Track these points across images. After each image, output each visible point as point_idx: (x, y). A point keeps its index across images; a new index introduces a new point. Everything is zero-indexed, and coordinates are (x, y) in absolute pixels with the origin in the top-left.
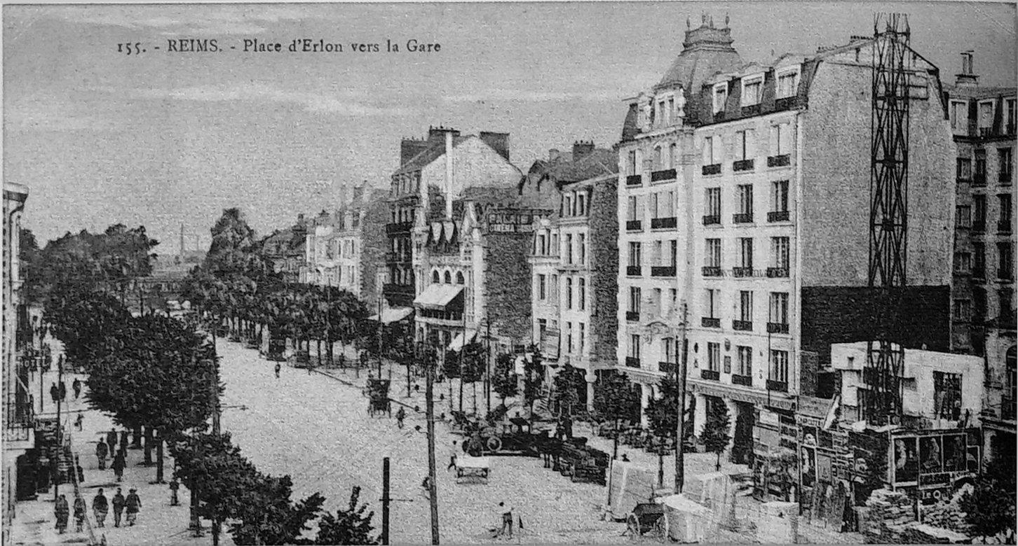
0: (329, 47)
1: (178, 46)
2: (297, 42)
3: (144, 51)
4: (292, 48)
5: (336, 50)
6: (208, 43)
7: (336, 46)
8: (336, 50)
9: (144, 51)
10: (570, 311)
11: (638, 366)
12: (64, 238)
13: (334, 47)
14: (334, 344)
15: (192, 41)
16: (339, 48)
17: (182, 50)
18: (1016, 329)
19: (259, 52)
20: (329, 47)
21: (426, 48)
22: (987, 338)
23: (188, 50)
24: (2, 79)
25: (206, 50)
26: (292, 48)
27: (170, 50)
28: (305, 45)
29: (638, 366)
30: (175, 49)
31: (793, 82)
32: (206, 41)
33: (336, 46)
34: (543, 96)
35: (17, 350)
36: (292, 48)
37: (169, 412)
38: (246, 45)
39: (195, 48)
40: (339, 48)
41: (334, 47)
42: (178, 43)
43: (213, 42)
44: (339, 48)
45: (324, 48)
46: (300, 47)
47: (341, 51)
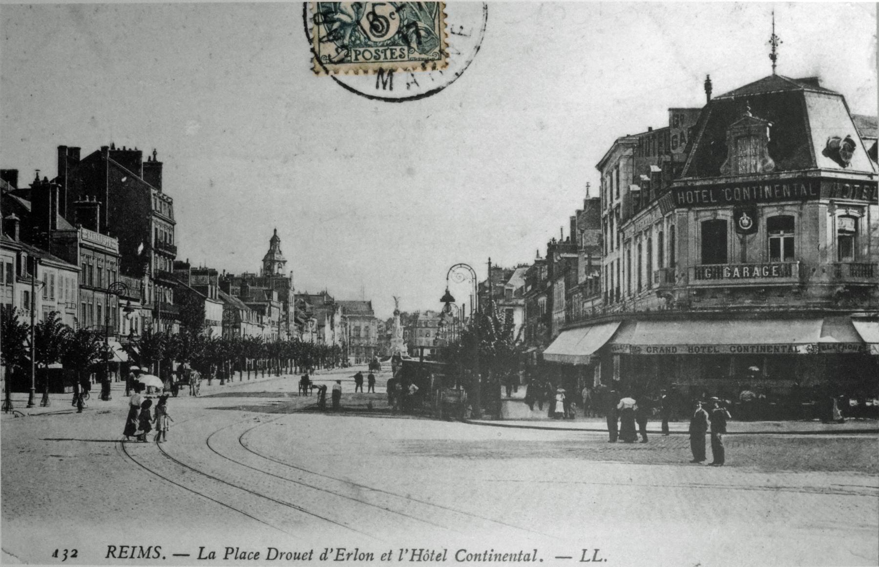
0: (362, 557)
1: (117, 553)
2: (329, 550)
3: (164, 558)
6: (152, 550)
9: (541, 560)
10: (587, 180)
12: (237, 279)
14: (109, 338)
15: (134, 547)
16: (370, 557)
17: (120, 557)
19: (358, 560)
20: (362, 557)
22: (127, 149)
25: (148, 557)
27: (108, 557)
28: (338, 554)
30: (114, 556)
32: (150, 548)
36: (324, 557)
37: (486, 353)
38: (227, 553)
39: (136, 555)
40: (370, 557)
42: (119, 549)
43: (158, 549)
46: (332, 556)
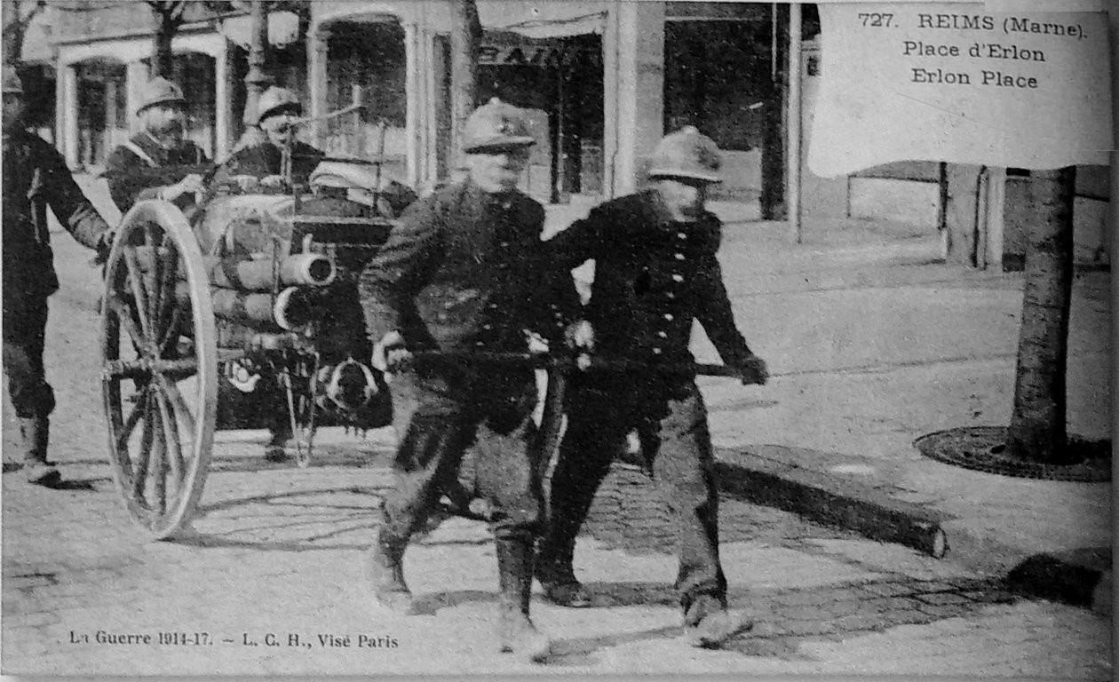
4: (974, 52)
5: (1035, 59)
6: (980, 20)
7: (115, 641)
8: (961, 82)
11: (292, 253)
13: (117, 640)
18: (768, 6)
21: (1042, 28)
23: (1000, 56)
24: (1116, 383)
26: (974, 52)
29: (292, 253)
31: (122, 220)
33: (1035, 53)
34: (774, 21)
35: (116, 435)
41: (117, 640)
44: (1039, 56)
45: (943, 79)
47: (968, 82)
